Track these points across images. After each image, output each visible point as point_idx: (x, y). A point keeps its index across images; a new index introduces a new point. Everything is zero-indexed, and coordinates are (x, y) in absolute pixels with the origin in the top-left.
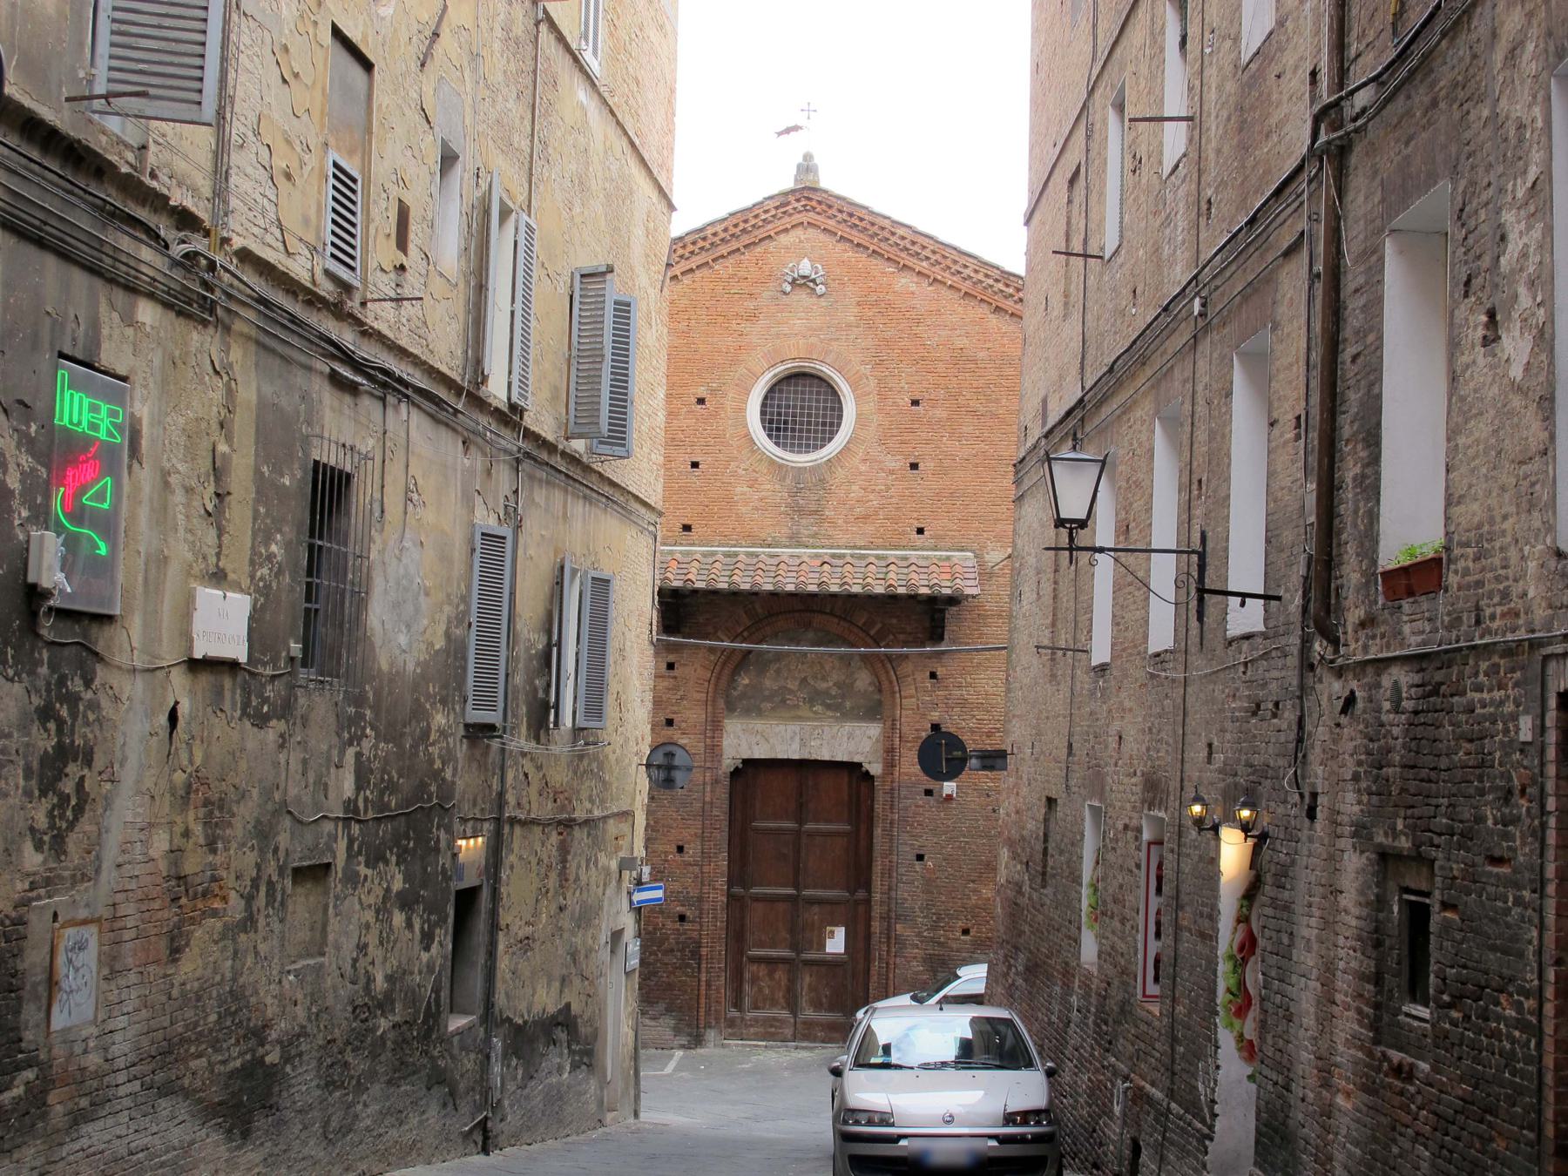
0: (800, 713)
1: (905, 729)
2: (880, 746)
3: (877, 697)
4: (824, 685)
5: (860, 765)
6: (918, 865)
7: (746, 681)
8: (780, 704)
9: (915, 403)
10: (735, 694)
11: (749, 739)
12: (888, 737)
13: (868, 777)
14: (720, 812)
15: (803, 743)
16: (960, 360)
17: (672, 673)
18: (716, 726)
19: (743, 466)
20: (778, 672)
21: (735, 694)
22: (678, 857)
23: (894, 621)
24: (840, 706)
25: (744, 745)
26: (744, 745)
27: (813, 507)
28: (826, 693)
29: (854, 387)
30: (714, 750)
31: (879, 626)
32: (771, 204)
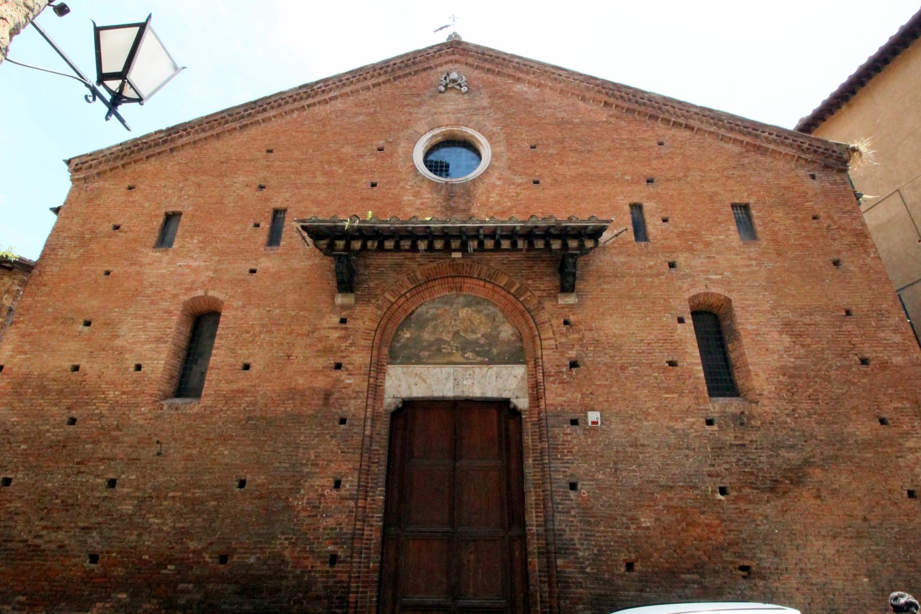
0: (453, 359)
1: (546, 365)
2: (525, 384)
3: (518, 344)
4: (473, 337)
5: (507, 402)
6: (572, 494)
7: (408, 335)
8: (435, 354)
9: (533, 147)
10: (398, 345)
11: (405, 382)
12: (532, 375)
13: (516, 413)
14: (380, 448)
15: (457, 383)
16: (561, 124)
17: (344, 326)
18: (377, 371)
19: (410, 183)
20: (435, 327)
21: (398, 345)
22: (335, 493)
23: (530, 282)
24: (489, 354)
25: (404, 386)
26: (404, 386)
27: (462, 207)
28: (476, 343)
29: (490, 138)
30: (376, 390)
31: (518, 285)
32: (107, 153)
